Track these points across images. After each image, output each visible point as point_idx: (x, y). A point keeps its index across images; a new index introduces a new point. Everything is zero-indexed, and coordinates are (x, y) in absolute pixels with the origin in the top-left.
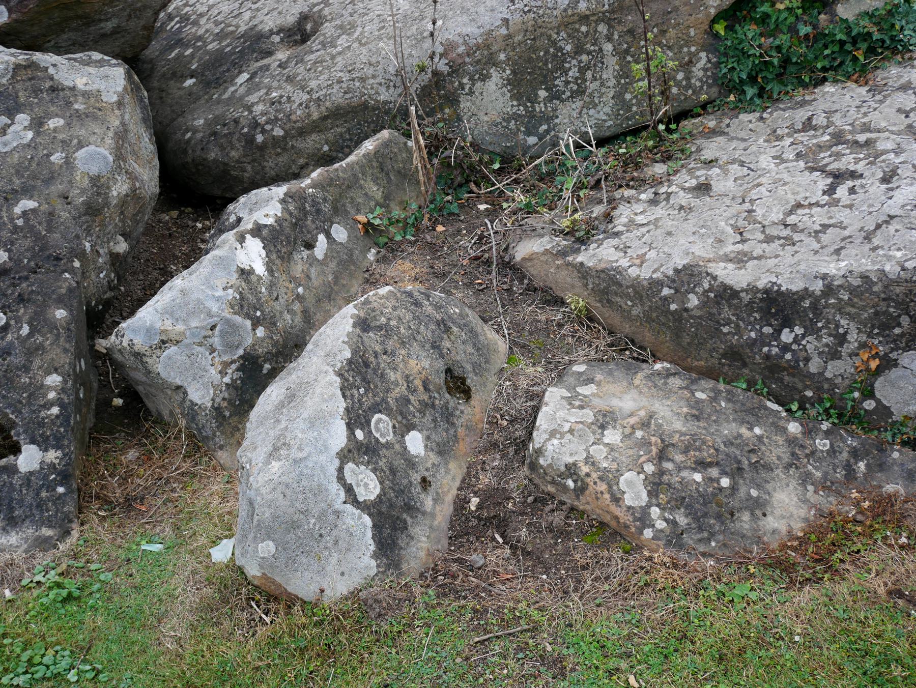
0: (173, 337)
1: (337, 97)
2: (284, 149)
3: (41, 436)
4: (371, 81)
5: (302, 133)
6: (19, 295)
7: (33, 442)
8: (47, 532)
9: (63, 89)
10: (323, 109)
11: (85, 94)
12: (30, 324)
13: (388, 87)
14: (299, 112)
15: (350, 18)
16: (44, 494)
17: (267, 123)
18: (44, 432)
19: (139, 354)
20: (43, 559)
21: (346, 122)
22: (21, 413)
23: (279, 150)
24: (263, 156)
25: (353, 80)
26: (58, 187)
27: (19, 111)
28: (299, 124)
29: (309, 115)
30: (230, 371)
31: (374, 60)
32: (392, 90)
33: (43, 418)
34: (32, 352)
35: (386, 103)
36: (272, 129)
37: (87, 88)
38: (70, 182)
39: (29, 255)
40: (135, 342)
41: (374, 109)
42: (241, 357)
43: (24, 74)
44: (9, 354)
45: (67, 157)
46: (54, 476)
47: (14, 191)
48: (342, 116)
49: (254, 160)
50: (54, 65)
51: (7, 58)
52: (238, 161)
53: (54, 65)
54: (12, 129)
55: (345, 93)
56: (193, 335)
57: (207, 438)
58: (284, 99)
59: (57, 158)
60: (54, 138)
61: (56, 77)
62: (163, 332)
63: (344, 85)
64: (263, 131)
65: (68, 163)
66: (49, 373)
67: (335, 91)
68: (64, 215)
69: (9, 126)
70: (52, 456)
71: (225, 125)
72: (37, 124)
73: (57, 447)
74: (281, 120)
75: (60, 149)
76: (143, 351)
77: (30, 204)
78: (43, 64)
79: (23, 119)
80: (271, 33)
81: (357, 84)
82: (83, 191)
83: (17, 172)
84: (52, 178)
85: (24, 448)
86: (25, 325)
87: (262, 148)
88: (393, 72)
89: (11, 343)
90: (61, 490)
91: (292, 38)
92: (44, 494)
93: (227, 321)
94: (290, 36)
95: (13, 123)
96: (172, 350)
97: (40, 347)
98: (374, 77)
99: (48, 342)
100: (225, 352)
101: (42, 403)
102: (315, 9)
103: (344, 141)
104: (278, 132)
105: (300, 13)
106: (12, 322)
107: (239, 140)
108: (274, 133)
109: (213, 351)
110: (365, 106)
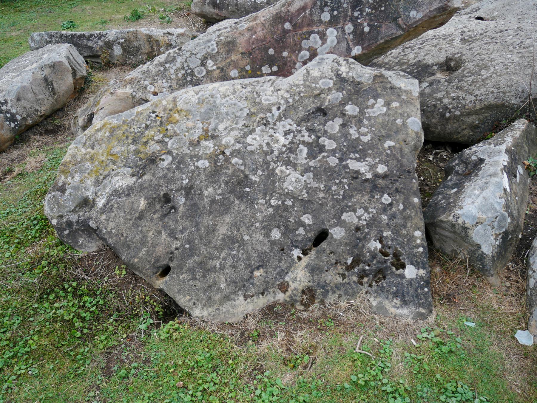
0: (481, 221)
1: (491, 100)
2: (458, 121)
3: (416, 261)
4: (508, 94)
5: (469, 114)
6: (396, 189)
7: (412, 264)
8: (423, 311)
9: (396, 88)
10: (483, 105)
11: (406, 92)
12: (403, 204)
13: (516, 98)
14: (470, 105)
15: (210, 49)
16: (419, 291)
17: (452, 108)
18: (417, 260)
19: (466, 228)
20: (422, 324)
21: (491, 111)
22: (404, 248)
23: (455, 121)
24: (447, 123)
25: (499, 92)
26: (401, 136)
27: (379, 98)
28: (469, 111)
29: (475, 107)
30: (499, 239)
31: (509, 84)
32: (518, 99)
33: (416, 253)
34: (406, 218)
35: (514, 104)
36: (455, 112)
37: (406, 89)
38: (407, 134)
39: (396, 168)
40: (466, 222)
41: (507, 107)
42: (503, 232)
43: (379, 80)
44: (395, 218)
45: (403, 122)
46: (423, 282)
47: (383, 136)
48: (490, 108)
49: (442, 124)
50: (390, 77)
51: (370, 71)
52: (435, 124)
53: (390, 77)
54: (376, 106)
55: (495, 98)
56: (489, 220)
57: (487, 270)
58: (461, 98)
59: (399, 121)
60: (396, 112)
61: (392, 82)
62: (479, 218)
63: (495, 95)
64: (450, 112)
65: (404, 124)
66: (416, 230)
67: (490, 97)
68: (407, 150)
69: (375, 104)
70: (422, 272)
71: (428, 107)
72: (388, 104)
73: (424, 268)
74: (460, 107)
75: (400, 117)
76: (469, 227)
77: (392, 144)
78: (386, 76)
79: (381, 101)
80: (433, 65)
81: (501, 95)
82: (413, 139)
83: (382, 127)
84: (398, 131)
85: (407, 266)
86: (401, 204)
87: (448, 119)
88: (520, 91)
89: (395, 213)
90: (426, 290)
91: (443, 68)
92: (419, 291)
93: (502, 215)
94: (441, 67)
95: (376, 103)
96: (479, 226)
97: (410, 216)
98: (510, 92)
99: (413, 214)
100: (497, 229)
101: (414, 245)
102: (456, 56)
103: (487, 120)
104: (458, 113)
105: (446, 57)
106: (394, 202)
107: (437, 115)
108: (456, 113)
109: (493, 228)
110: (503, 105)
